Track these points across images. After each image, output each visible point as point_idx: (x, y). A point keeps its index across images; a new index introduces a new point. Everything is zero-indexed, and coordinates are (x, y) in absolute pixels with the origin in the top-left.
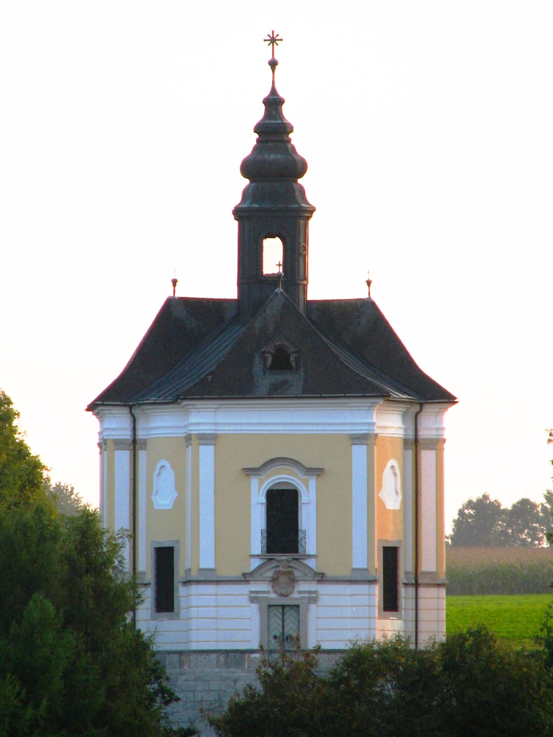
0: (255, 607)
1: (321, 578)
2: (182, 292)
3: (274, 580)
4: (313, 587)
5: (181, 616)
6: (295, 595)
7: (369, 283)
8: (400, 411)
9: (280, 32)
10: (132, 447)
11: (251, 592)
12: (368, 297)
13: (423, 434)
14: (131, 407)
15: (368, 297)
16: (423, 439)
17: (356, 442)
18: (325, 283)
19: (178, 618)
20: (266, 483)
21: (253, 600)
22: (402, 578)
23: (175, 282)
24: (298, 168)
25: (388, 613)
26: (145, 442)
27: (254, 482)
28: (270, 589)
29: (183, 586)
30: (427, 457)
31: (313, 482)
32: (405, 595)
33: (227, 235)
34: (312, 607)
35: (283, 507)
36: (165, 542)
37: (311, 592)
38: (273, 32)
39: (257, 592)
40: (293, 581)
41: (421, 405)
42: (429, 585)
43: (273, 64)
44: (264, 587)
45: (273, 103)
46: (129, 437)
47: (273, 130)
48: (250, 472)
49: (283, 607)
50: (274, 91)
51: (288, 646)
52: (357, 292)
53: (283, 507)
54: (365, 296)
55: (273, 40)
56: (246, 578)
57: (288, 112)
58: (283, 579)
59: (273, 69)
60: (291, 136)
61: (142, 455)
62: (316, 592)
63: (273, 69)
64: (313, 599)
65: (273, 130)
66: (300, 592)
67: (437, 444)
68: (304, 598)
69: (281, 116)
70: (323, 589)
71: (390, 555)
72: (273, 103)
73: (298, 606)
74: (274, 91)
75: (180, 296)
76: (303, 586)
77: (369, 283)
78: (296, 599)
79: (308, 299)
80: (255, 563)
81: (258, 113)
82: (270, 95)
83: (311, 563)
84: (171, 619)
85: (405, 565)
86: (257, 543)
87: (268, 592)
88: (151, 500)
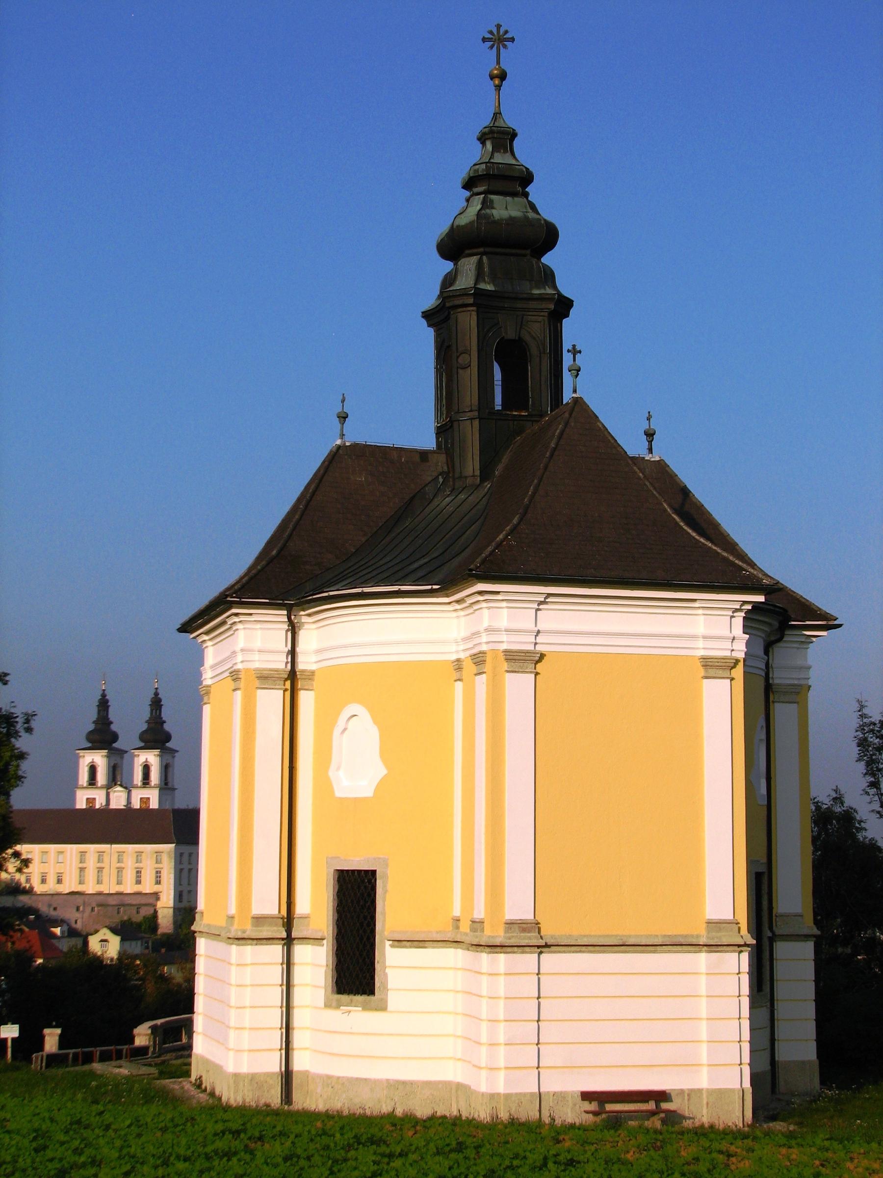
2: (359, 433)
5: (391, 1005)
8: (770, 624)
10: (288, 684)
13: (779, 677)
17: (712, 672)
19: (382, 1007)
25: (345, 998)
26: (311, 675)
29: (392, 946)
30: (783, 712)
36: (356, 862)
46: (282, 666)
55: (499, 39)
61: (305, 699)
67: (798, 693)
75: (361, 440)
84: (366, 1008)
85: (315, 962)
88: (328, 779)
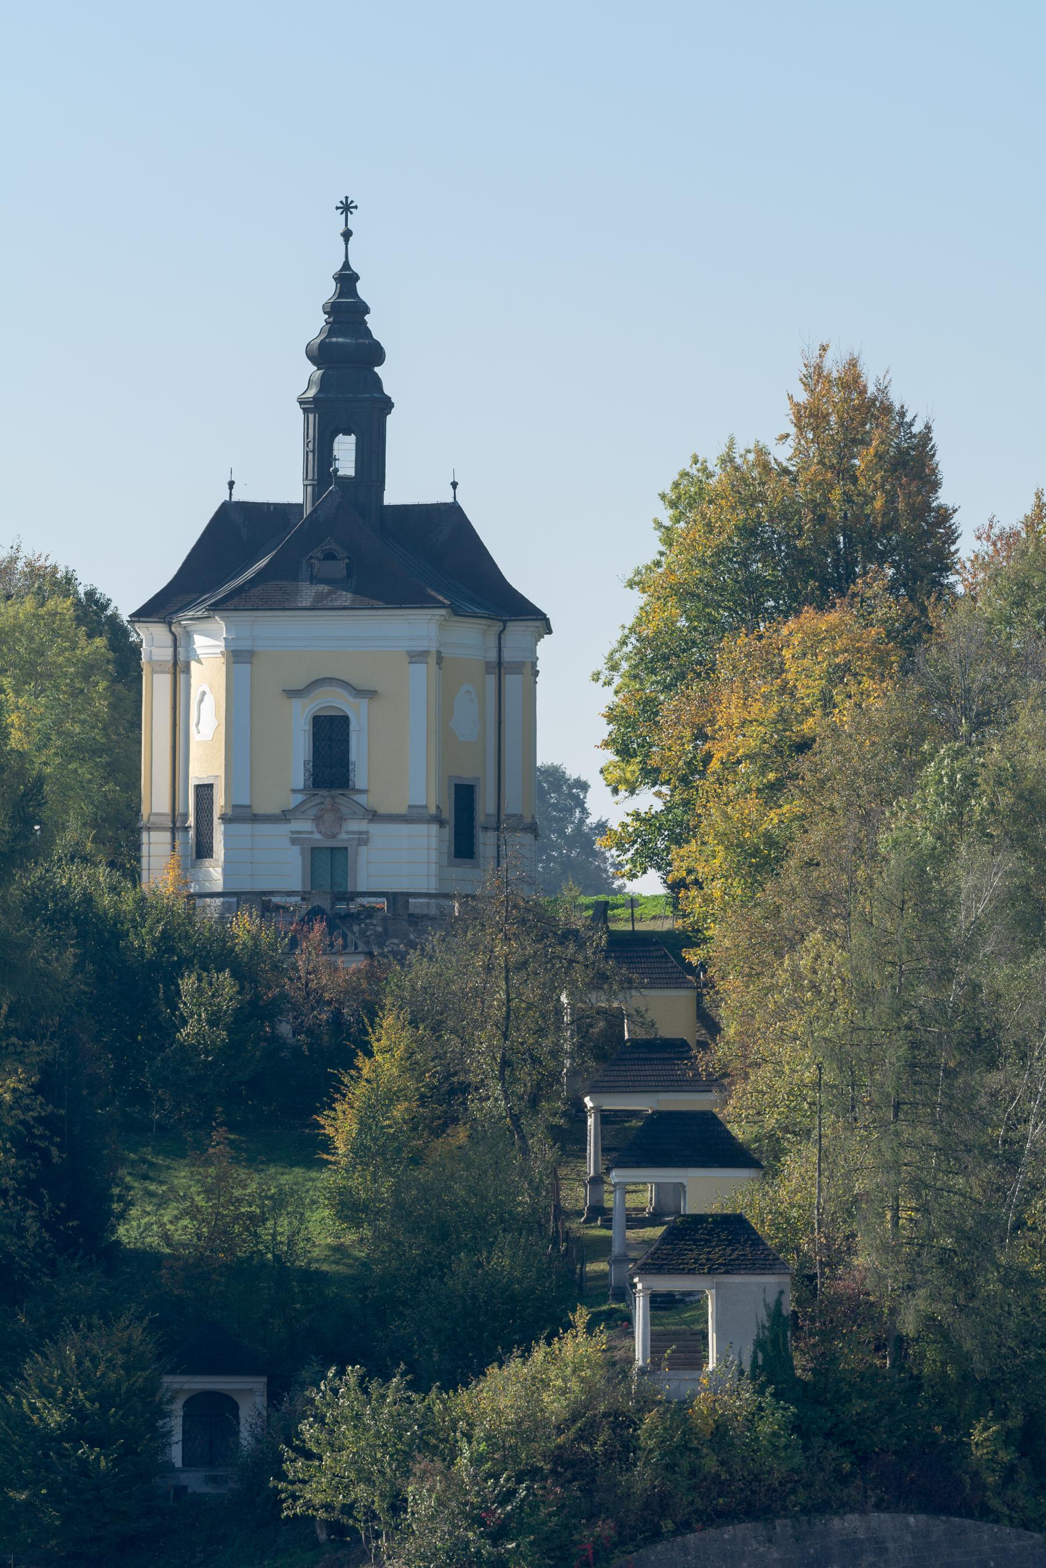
0: (297, 849)
1: (374, 816)
2: (240, 495)
3: (317, 819)
4: (363, 825)
6: (343, 836)
7: (454, 485)
9: (355, 198)
11: (292, 832)
12: (452, 500)
13: (508, 656)
14: (170, 624)
15: (452, 500)
16: (508, 662)
17: (414, 659)
18: (405, 486)
20: (308, 709)
21: (293, 842)
22: (480, 818)
23: (231, 484)
24: (376, 354)
27: (296, 703)
28: (315, 830)
30: (511, 681)
31: (364, 703)
32: (485, 842)
33: (292, 431)
34: (363, 849)
35: (330, 737)
37: (361, 833)
38: (347, 198)
39: (299, 832)
40: (341, 819)
41: (505, 622)
42: (514, 830)
43: (347, 235)
44: (304, 825)
45: (347, 279)
47: (347, 310)
48: (292, 694)
49: (332, 849)
50: (346, 265)
51: (921, 1055)
52: (439, 495)
53: (330, 737)
54: (450, 500)
55: (347, 207)
56: (285, 817)
57: (363, 290)
58: (328, 817)
59: (347, 241)
60: (367, 318)
62: (367, 833)
63: (347, 241)
64: (363, 840)
65: (347, 310)
66: (348, 833)
68: (353, 839)
69: (355, 295)
70: (376, 830)
71: (464, 796)
72: (347, 279)
73: (346, 849)
74: (346, 265)
76: (354, 826)
77: (454, 485)
78: (345, 840)
79: (386, 502)
80: (300, 798)
81: (328, 290)
82: (341, 270)
83: (361, 799)
85: (485, 805)
86: (298, 774)
87: (312, 833)
